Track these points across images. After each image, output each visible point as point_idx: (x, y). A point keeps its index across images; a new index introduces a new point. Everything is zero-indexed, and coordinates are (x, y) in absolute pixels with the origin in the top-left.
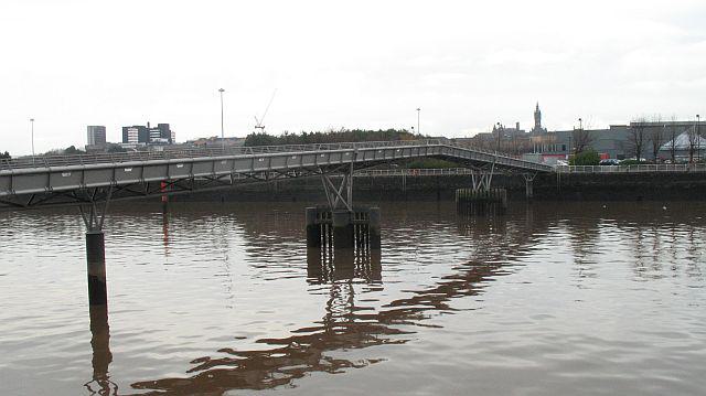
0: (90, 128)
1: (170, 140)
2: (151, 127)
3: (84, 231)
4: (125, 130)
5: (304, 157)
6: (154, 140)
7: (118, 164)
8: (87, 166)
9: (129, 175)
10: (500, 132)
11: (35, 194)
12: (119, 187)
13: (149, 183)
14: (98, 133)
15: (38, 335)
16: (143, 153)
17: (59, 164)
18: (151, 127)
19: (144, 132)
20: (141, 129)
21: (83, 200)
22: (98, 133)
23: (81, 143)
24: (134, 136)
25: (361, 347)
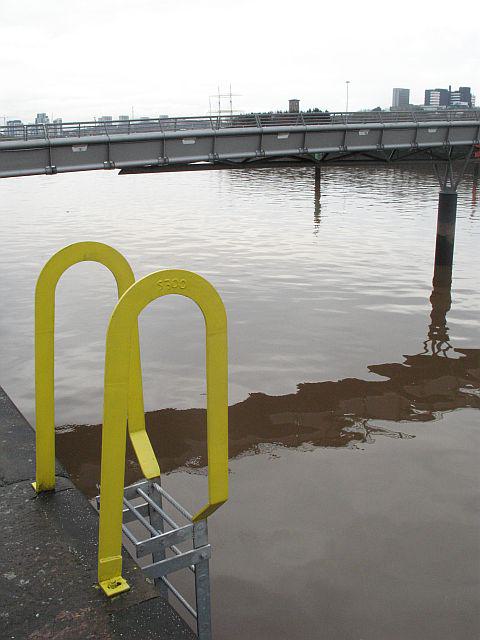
0: (395, 90)
1: (470, 104)
2: (452, 90)
3: (438, 190)
4: (428, 93)
5: (451, 131)
6: (454, 103)
7: (421, 124)
8: (387, 125)
9: (430, 138)
10: (294, 114)
11: (396, 150)
12: (420, 150)
13: (453, 146)
14: (402, 95)
15: (417, 295)
16: (443, 115)
17: (405, 120)
18: (452, 90)
19: (446, 95)
20: (442, 92)
21: (439, 158)
22: (402, 95)
23: (386, 104)
24: (436, 99)
25: (340, 442)
